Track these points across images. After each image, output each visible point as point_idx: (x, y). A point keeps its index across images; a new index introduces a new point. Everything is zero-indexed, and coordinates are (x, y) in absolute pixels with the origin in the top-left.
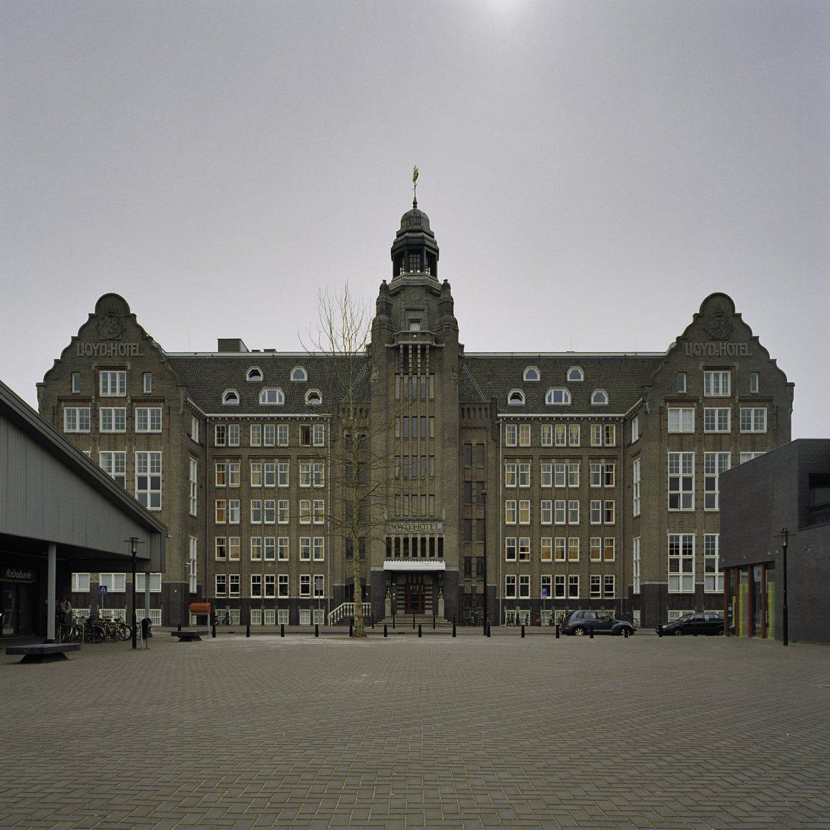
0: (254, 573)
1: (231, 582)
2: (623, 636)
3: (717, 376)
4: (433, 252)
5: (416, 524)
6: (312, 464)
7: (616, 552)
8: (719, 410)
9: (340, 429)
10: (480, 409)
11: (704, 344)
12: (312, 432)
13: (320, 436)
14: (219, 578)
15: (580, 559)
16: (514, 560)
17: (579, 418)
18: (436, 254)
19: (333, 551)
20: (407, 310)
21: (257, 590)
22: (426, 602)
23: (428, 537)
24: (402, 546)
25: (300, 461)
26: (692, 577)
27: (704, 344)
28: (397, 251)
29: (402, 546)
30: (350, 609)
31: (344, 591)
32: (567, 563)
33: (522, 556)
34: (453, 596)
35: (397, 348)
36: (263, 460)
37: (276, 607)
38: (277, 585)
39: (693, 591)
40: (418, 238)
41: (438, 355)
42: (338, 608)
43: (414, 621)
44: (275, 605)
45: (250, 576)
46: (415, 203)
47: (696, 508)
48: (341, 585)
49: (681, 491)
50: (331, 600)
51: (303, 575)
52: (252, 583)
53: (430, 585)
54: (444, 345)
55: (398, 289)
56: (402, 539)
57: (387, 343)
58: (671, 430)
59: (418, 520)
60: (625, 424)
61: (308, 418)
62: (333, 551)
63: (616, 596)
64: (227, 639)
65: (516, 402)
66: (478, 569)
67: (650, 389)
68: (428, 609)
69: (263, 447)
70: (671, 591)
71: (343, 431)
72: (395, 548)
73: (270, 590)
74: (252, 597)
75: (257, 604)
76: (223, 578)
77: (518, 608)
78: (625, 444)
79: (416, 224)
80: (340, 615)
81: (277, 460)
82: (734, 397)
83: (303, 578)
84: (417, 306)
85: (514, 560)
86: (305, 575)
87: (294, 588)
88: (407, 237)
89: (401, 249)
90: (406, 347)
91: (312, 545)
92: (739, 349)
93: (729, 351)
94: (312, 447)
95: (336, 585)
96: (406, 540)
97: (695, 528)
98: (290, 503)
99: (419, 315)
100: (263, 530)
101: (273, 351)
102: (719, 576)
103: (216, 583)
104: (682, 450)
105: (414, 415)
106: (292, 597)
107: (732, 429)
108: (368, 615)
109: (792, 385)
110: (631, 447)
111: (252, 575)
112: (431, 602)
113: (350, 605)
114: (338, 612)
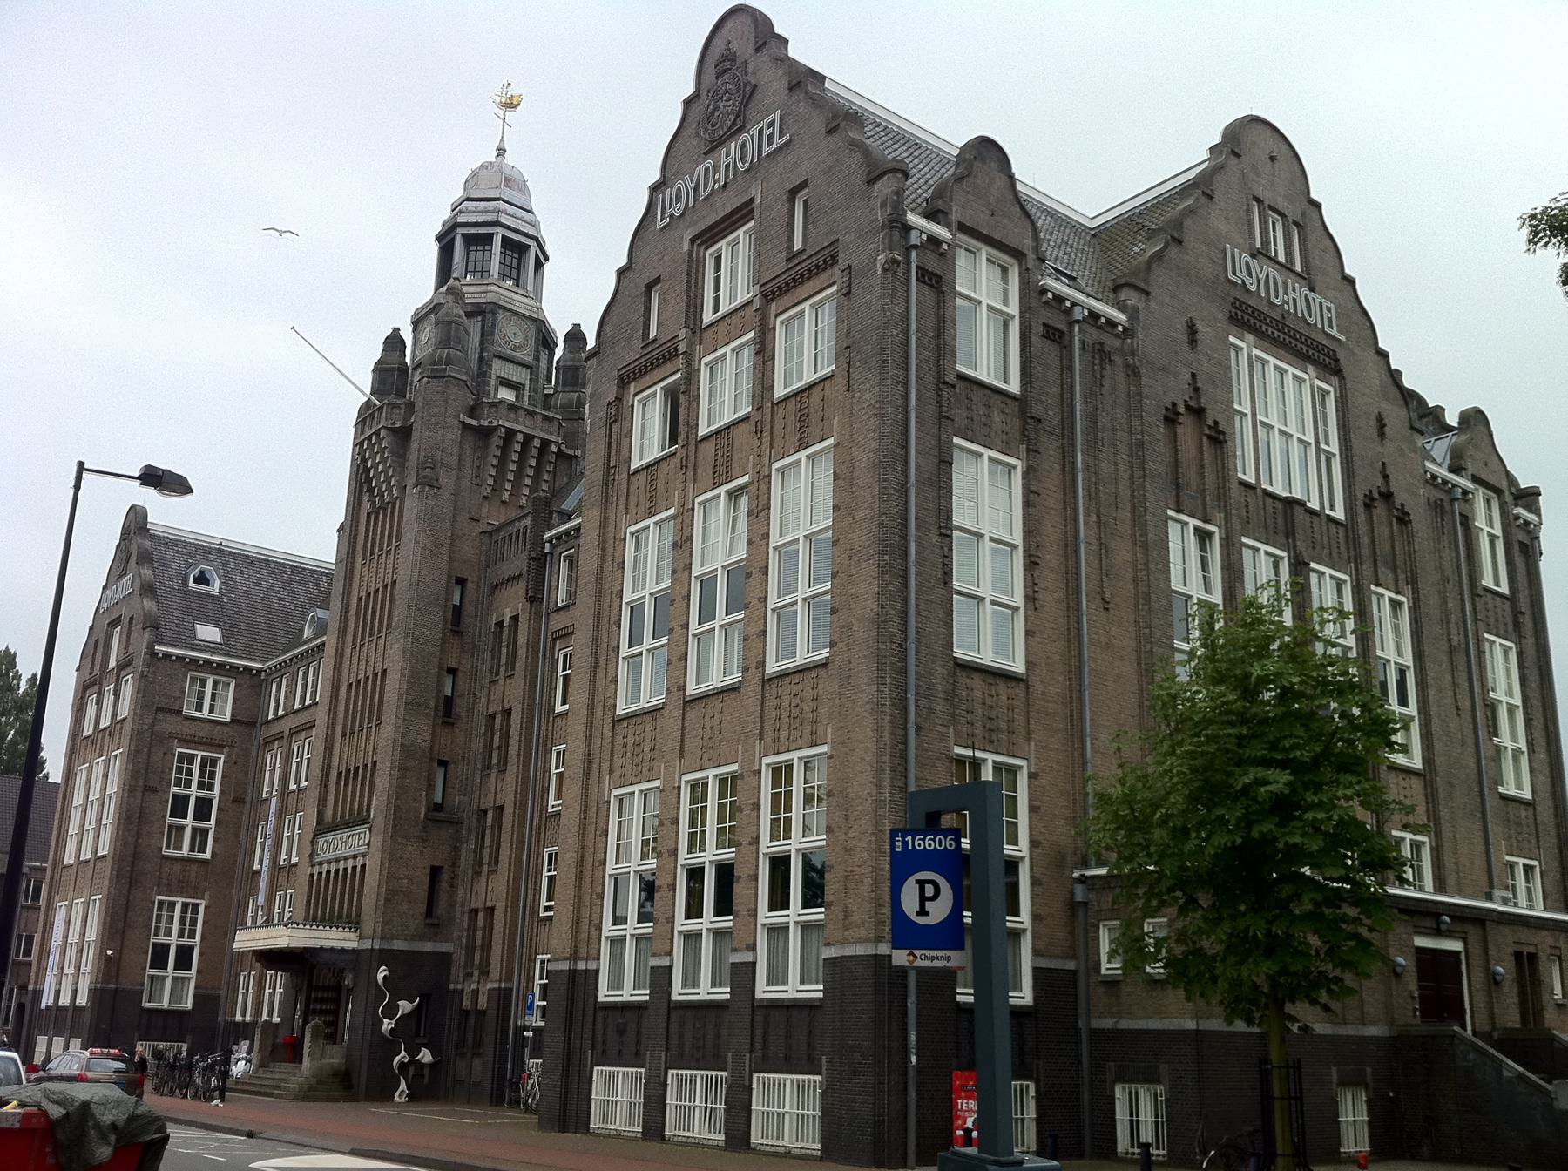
35: (485, 433)
46: (501, 152)
90: (511, 433)
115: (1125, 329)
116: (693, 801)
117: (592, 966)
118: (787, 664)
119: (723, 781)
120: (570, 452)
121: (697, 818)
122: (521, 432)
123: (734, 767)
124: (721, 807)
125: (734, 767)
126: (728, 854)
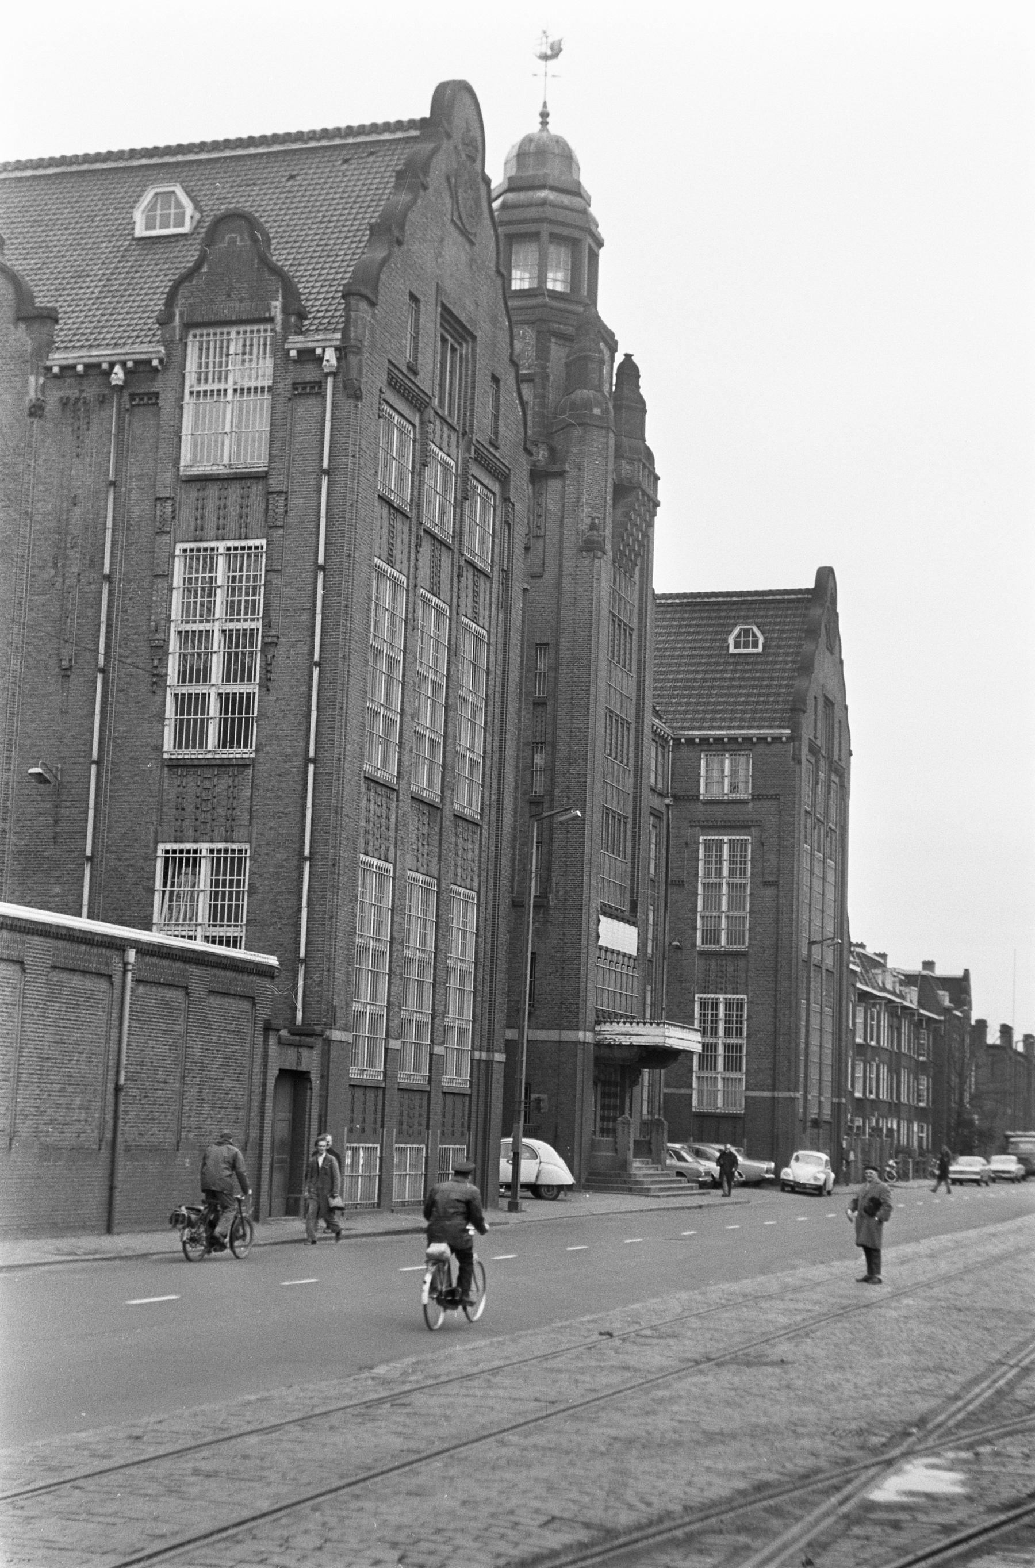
46: (544, 115)
115: (161, 361)
117: (477, 1055)
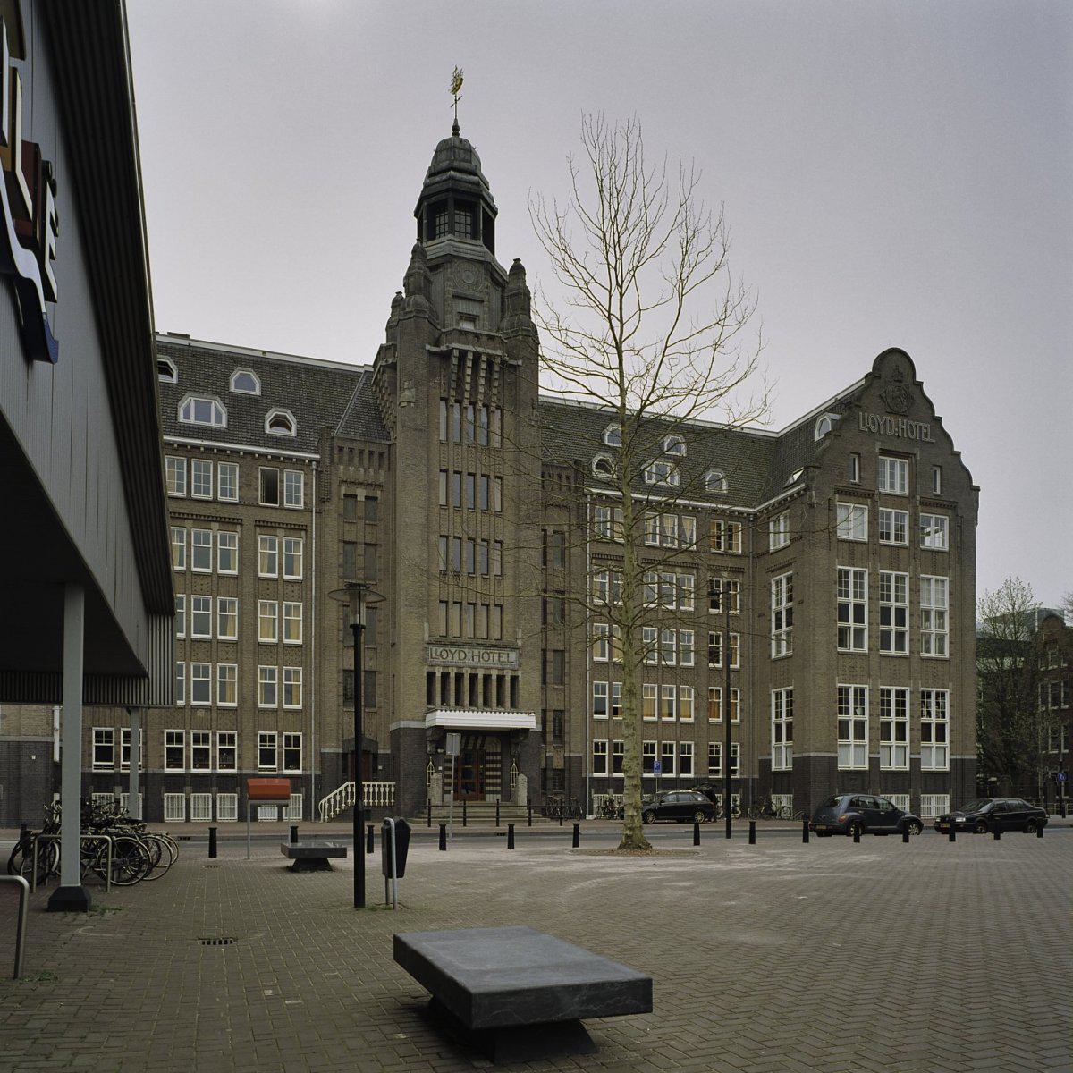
0: (171, 727)
1: (124, 742)
2: (852, 839)
3: (892, 465)
4: (490, 213)
5: (476, 652)
6: (280, 538)
7: (741, 710)
8: (896, 513)
9: (335, 486)
10: (560, 477)
11: (881, 418)
12: (282, 481)
13: (297, 490)
14: (99, 734)
15: (695, 718)
16: (606, 717)
17: (695, 508)
18: (493, 217)
19: (319, 692)
20: (456, 296)
21: (175, 757)
22: (488, 781)
23: (494, 674)
24: (452, 686)
25: (258, 529)
26: (864, 746)
27: (881, 418)
28: (434, 199)
29: (452, 686)
30: (374, 792)
31: (341, 762)
32: (678, 724)
33: (615, 712)
34: (536, 774)
35: (446, 356)
36: (189, 523)
37: (215, 789)
38: (214, 748)
39: (867, 767)
40: (469, 183)
41: (509, 378)
42: (332, 795)
43: (465, 812)
44: (185, 785)
45: (163, 733)
46: (456, 129)
47: (911, 652)
48: (337, 750)
49: (851, 624)
50: (316, 776)
51: (263, 733)
52: (166, 745)
53: (496, 754)
54: (520, 363)
55: (440, 261)
56: (452, 675)
57: (430, 344)
58: (841, 534)
59: (479, 645)
60: (757, 526)
61: (275, 457)
62: (319, 692)
63: (741, 773)
64: (709, 867)
65: (604, 476)
66: (554, 729)
67: (818, 471)
68: (493, 792)
69: (189, 499)
70: (841, 766)
71: (339, 486)
72: (443, 689)
73: (202, 757)
74: (167, 770)
75: (176, 783)
76: (109, 735)
77: (118, 789)
78: (759, 554)
79: (464, 160)
80: (341, 803)
81: (215, 526)
82: (914, 497)
83: (263, 739)
84: (472, 293)
85: (606, 717)
86: (268, 733)
87: (248, 755)
88: (452, 178)
89: (443, 196)
90: (463, 354)
91: (280, 679)
92: (921, 430)
93: (910, 434)
94: (282, 508)
95: (326, 750)
96: (459, 677)
97: (869, 676)
98: (241, 603)
99: (474, 309)
100: (188, 649)
101: (187, 337)
102: (937, 748)
103: (94, 744)
104: (853, 566)
105: (470, 471)
106: (245, 772)
107: (910, 541)
108: (390, 802)
109: (977, 489)
110: (767, 557)
111: (166, 731)
112: (499, 781)
113: (385, 786)
114: (344, 794)
116: (777, 699)
118: (779, 656)
119: (788, 578)
120: (513, 362)
121: (778, 706)
122: (470, 351)
123: (791, 687)
124: (787, 702)
125: (791, 687)
126: (790, 719)
